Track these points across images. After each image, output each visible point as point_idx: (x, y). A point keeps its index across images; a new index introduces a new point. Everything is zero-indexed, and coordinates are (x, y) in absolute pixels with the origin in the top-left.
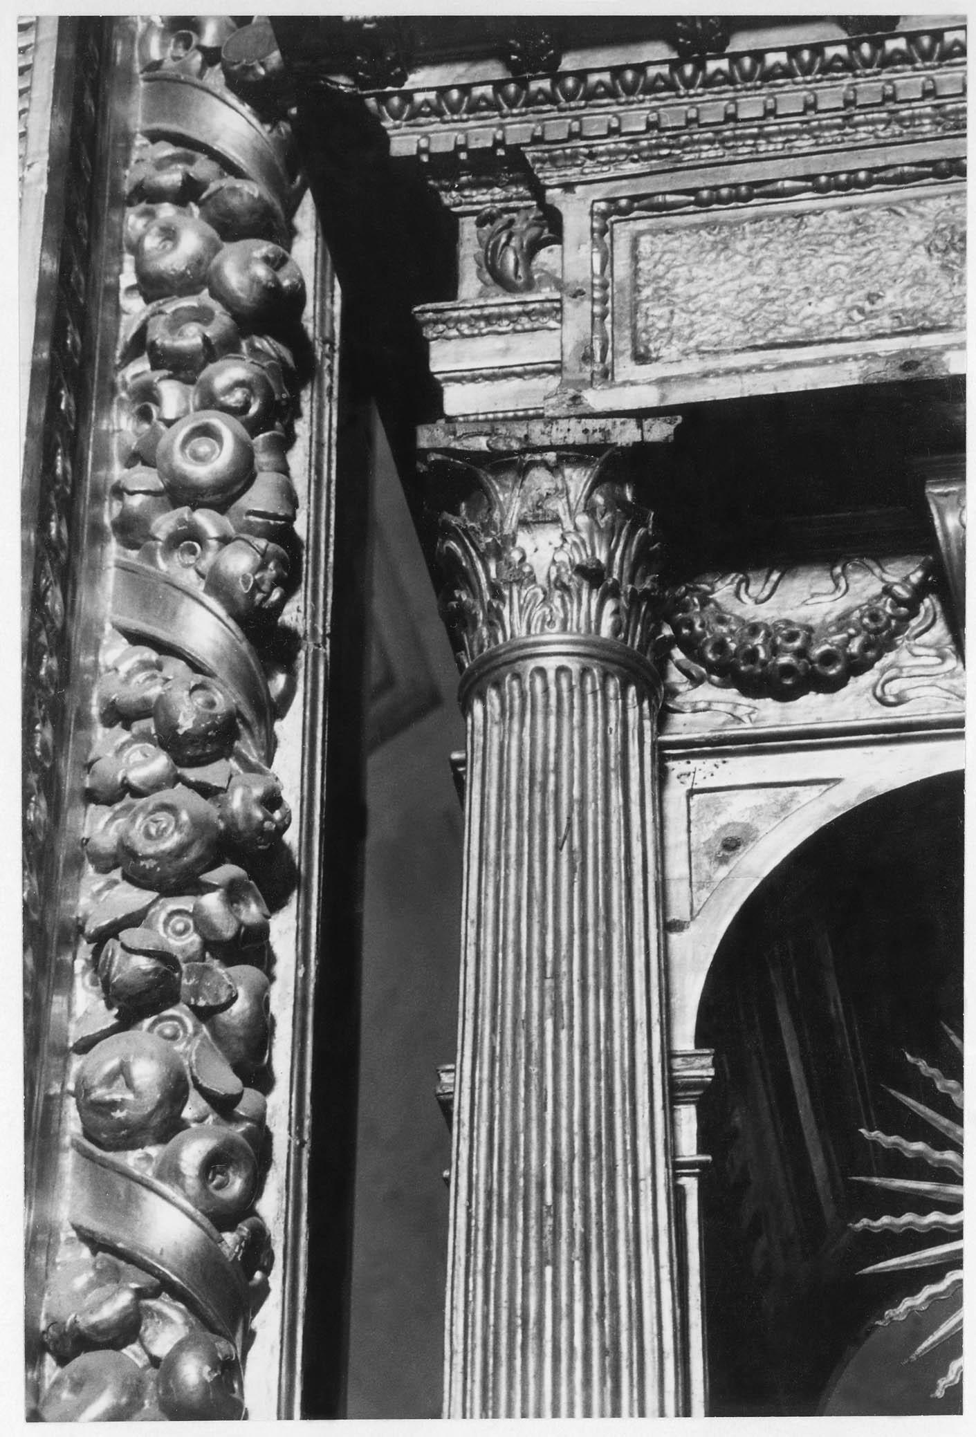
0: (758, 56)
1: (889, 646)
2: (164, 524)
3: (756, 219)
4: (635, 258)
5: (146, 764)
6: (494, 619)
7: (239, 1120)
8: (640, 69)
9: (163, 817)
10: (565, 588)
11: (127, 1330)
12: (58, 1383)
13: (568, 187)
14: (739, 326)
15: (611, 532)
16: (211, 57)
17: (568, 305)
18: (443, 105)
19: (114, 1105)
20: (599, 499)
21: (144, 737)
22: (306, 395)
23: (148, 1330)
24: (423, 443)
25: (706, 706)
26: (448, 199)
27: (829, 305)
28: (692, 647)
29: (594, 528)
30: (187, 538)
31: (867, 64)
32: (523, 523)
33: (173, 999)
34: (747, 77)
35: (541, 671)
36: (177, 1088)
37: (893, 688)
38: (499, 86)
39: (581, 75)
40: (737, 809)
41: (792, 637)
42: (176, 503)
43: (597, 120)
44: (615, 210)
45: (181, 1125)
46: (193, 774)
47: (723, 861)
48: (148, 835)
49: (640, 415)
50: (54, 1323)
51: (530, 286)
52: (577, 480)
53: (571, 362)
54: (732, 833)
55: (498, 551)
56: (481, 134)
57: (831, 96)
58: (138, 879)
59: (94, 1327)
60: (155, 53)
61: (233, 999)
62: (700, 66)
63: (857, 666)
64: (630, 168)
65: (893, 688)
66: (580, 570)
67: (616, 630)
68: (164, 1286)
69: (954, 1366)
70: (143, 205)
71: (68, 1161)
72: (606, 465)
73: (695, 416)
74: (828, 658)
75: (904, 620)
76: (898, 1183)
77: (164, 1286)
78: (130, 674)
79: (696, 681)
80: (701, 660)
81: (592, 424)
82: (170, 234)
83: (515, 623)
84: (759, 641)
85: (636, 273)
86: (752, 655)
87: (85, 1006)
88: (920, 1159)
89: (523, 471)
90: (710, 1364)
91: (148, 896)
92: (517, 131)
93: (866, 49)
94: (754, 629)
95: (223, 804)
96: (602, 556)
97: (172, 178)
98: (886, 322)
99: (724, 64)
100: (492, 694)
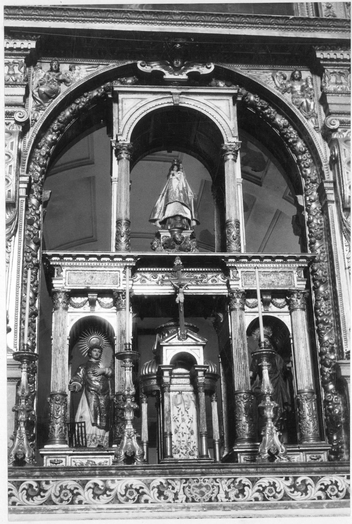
18: (54, 261)
25: (71, 309)
28: (70, 304)
40: (73, 317)
44: (67, 270)
52: (64, 294)
56: (57, 263)
63: (82, 306)
69: (256, 332)
87: (241, 500)
90: (230, 350)
92: (60, 264)
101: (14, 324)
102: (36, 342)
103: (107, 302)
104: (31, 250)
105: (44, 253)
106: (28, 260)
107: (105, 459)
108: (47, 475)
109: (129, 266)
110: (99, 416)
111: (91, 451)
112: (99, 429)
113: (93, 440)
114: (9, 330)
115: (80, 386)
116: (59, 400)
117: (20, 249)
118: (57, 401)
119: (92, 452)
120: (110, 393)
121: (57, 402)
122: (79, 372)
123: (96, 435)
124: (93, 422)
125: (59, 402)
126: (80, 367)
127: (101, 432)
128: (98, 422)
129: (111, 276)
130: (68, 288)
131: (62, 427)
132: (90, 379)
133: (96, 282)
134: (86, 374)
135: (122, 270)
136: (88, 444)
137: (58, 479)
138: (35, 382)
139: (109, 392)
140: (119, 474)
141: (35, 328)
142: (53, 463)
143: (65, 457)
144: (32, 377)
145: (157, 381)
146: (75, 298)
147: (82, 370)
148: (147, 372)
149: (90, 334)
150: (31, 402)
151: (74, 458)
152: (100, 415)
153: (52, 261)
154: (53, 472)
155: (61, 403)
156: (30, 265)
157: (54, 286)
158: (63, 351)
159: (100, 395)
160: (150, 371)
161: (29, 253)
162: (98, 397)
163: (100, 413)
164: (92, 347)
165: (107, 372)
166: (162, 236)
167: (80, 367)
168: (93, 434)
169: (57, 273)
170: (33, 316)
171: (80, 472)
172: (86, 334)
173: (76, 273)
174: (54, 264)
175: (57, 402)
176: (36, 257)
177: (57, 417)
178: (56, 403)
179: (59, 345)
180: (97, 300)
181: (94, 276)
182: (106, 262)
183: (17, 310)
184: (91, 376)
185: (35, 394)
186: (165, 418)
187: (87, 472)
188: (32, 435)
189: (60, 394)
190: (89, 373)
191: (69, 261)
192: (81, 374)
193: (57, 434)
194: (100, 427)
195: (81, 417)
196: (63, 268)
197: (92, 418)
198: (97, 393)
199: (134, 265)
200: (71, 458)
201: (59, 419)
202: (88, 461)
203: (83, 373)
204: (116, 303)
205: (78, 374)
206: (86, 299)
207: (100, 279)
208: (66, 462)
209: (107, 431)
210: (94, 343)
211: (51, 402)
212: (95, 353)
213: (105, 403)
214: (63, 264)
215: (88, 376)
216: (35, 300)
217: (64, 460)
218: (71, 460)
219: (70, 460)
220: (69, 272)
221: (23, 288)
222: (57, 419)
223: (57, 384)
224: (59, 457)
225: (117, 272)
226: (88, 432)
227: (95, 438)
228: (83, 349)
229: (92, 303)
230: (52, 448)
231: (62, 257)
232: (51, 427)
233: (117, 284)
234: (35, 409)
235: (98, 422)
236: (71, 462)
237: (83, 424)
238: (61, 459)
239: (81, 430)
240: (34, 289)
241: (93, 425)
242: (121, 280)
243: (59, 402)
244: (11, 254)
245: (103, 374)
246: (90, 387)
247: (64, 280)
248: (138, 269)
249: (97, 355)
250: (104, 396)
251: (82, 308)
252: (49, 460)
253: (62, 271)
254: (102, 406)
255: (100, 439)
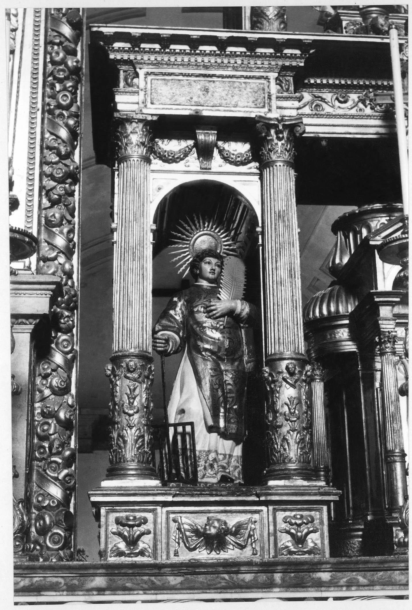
0: (175, 50)
1: (187, 156)
2: (57, 112)
3: (172, 80)
4: (151, 84)
5: (54, 158)
6: (126, 149)
7: (72, 224)
8: (154, 49)
9: (59, 170)
10: (138, 145)
11: (55, 259)
12: (44, 266)
13: (140, 69)
14: (168, 100)
15: (146, 136)
16: (64, 15)
17: (140, 92)
18: (119, 50)
19: (52, 221)
20: (144, 130)
21: (54, 153)
22: (79, 85)
23: (59, 259)
24: (115, 116)
25: (157, 164)
26: (119, 66)
27: (184, 98)
29: (143, 134)
30: (61, 115)
31: (193, 54)
32: (131, 132)
33: (60, 203)
34: (172, 53)
35: (134, 160)
36: (63, 217)
37: (187, 164)
38: (129, 48)
39: (144, 48)
40: (160, 183)
41: (172, 154)
42: (59, 109)
43: (146, 57)
44: (147, 74)
45: (62, 224)
46: (63, 162)
47: (158, 191)
48: (57, 173)
49: (152, 115)
50: (43, 256)
51: (132, 86)
52: (141, 125)
53: (140, 103)
54: (160, 187)
55: (127, 137)
57: (186, 59)
58: (55, 181)
59: (51, 258)
60: (53, 12)
61: (71, 204)
62: (164, 50)
63: (182, 159)
64: (151, 67)
65: (187, 164)
66: (141, 143)
67: (146, 153)
68: (61, 252)
70: (51, 45)
71: (43, 228)
72: (146, 123)
73: (162, 117)
74: (177, 158)
75: (190, 152)
76: (176, 240)
77: (61, 252)
78: (51, 140)
79: (155, 159)
80: (156, 155)
81: (144, 115)
82: (58, 53)
83: (129, 151)
84: (166, 153)
85: (151, 87)
86: (165, 156)
88: (180, 237)
89: (131, 123)
91: (56, 184)
92: (132, 57)
93: (193, 52)
94: (165, 151)
95: (70, 168)
96: (144, 140)
97: (57, 41)
98: (193, 103)
99: (168, 50)
100: (125, 163)
101: (25, 191)
102: (76, 239)
103: (238, 152)
104: (63, 39)
105: (95, 29)
106: (57, 59)
107: (249, 516)
108: (128, 585)
109: (290, 68)
110: (222, 410)
111: (217, 495)
112: (221, 439)
113: (212, 466)
114: (14, 204)
115: (176, 342)
116: (135, 370)
117: (39, 26)
118: (129, 371)
119: (217, 499)
120: (246, 358)
121: (129, 375)
122: (174, 309)
123: (216, 451)
124: (210, 422)
125: (136, 375)
126: (175, 299)
127: (226, 446)
128: (222, 424)
129: (248, 90)
130: (153, 110)
131: (143, 436)
132: (199, 324)
133: (216, 102)
134: (190, 313)
135: (273, 75)
136: (200, 474)
137: (160, 597)
138: (74, 330)
139: (242, 356)
140: (343, 582)
141: (74, 208)
142: (123, 525)
143: (153, 511)
144: (67, 316)
145: (350, 332)
146: (166, 140)
147: (179, 304)
148: (325, 312)
149: (195, 226)
150: (65, 375)
151: (174, 512)
152: (225, 408)
153: (114, 51)
154: (146, 578)
155: (140, 376)
156: (59, 70)
157: (119, 107)
158: (142, 257)
159: (223, 360)
160: (333, 309)
161: (58, 44)
162: (218, 366)
163: (226, 402)
164: (200, 257)
165: (238, 310)
166: (344, 23)
167: (175, 299)
168: (209, 451)
169: (126, 80)
170: (69, 180)
171: (226, 576)
172: (188, 228)
173: (168, 80)
174: (119, 57)
175: (129, 375)
176: (74, 53)
177: (131, 412)
178: (126, 377)
179: (133, 241)
180: (216, 145)
181: (211, 86)
182: (237, 56)
183: (31, 158)
184: (202, 317)
185: (74, 358)
186: (387, 414)
187: (248, 577)
188: (68, 453)
189: (137, 356)
190: (198, 312)
191: (152, 51)
192: (177, 313)
193: (130, 452)
194: (224, 435)
195: (182, 411)
196: (138, 66)
197: (208, 414)
198: (217, 356)
199: (302, 64)
200: (168, 513)
201: (136, 416)
202: (208, 518)
203: (182, 313)
204: (260, 157)
205: (172, 312)
206: (191, 142)
207: (224, 94)
208: (155, 522)
209: (237, 444)
210: (204, 247)
211: (115, 376)
212: (208, 267)
213: (234, 379)
214: (139, 57)
215: (194, 319)
216: (74, 148)
217: (150, 516)
218: (167, 518)
219: (164, 516)
220: (153, 77)
221: (46, 121)
222: (130, 415)
223: (129, 331)
224: (139, 511)
225: (262, 81)
226: (198, 447)
227: (215, 460)
228: (180, 260)
229: (205, 152)
230: (120, 488)
231: (135, 42)
232: (115, 435)
233: (264, 107)
234: (73, 391)
235: (222, 424)
236: (168, 523)
237: (188, 429)
238: (143, 515)
239: (184, 441)
240: (71, 122)
241: (210, 429)
242: (273, 97)
243: (136, 375)
244: (19, 33)
245: (231, 313)
246: (199, 343)
247: (142, 93)
248: (306, 81)
249: (213, 271)
250: (232, 364)
251: (182, 162)
252: (112, 517)
253: (137, 75)
254: (229, 387)
255: (224, 463)
